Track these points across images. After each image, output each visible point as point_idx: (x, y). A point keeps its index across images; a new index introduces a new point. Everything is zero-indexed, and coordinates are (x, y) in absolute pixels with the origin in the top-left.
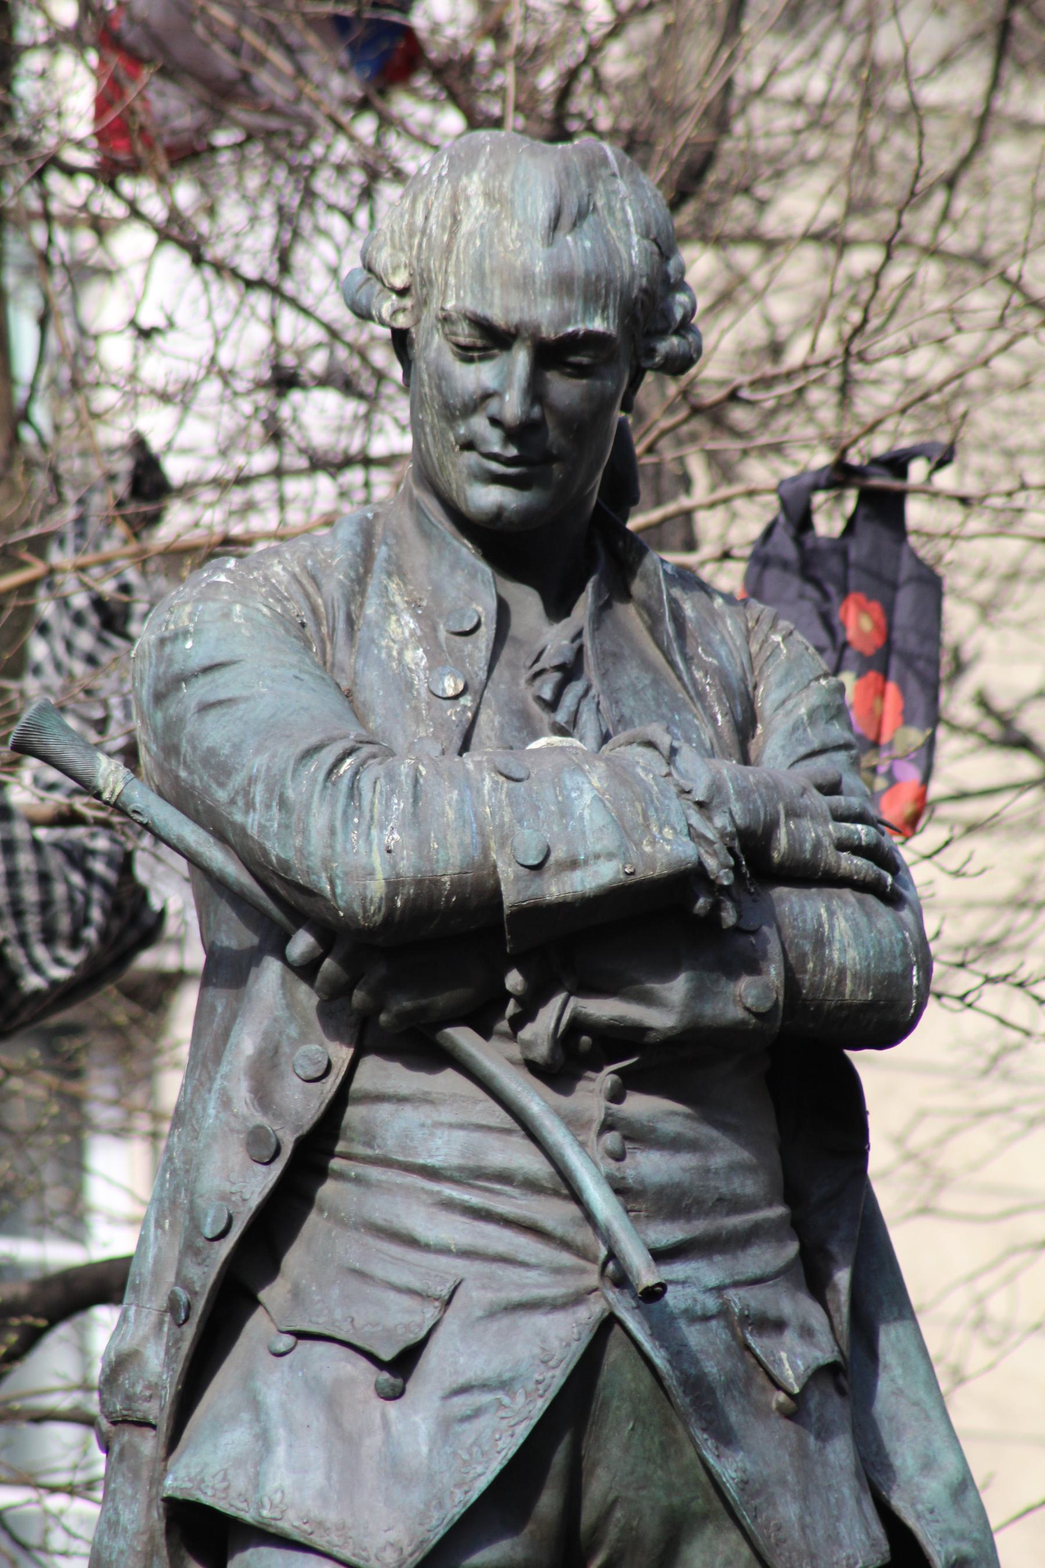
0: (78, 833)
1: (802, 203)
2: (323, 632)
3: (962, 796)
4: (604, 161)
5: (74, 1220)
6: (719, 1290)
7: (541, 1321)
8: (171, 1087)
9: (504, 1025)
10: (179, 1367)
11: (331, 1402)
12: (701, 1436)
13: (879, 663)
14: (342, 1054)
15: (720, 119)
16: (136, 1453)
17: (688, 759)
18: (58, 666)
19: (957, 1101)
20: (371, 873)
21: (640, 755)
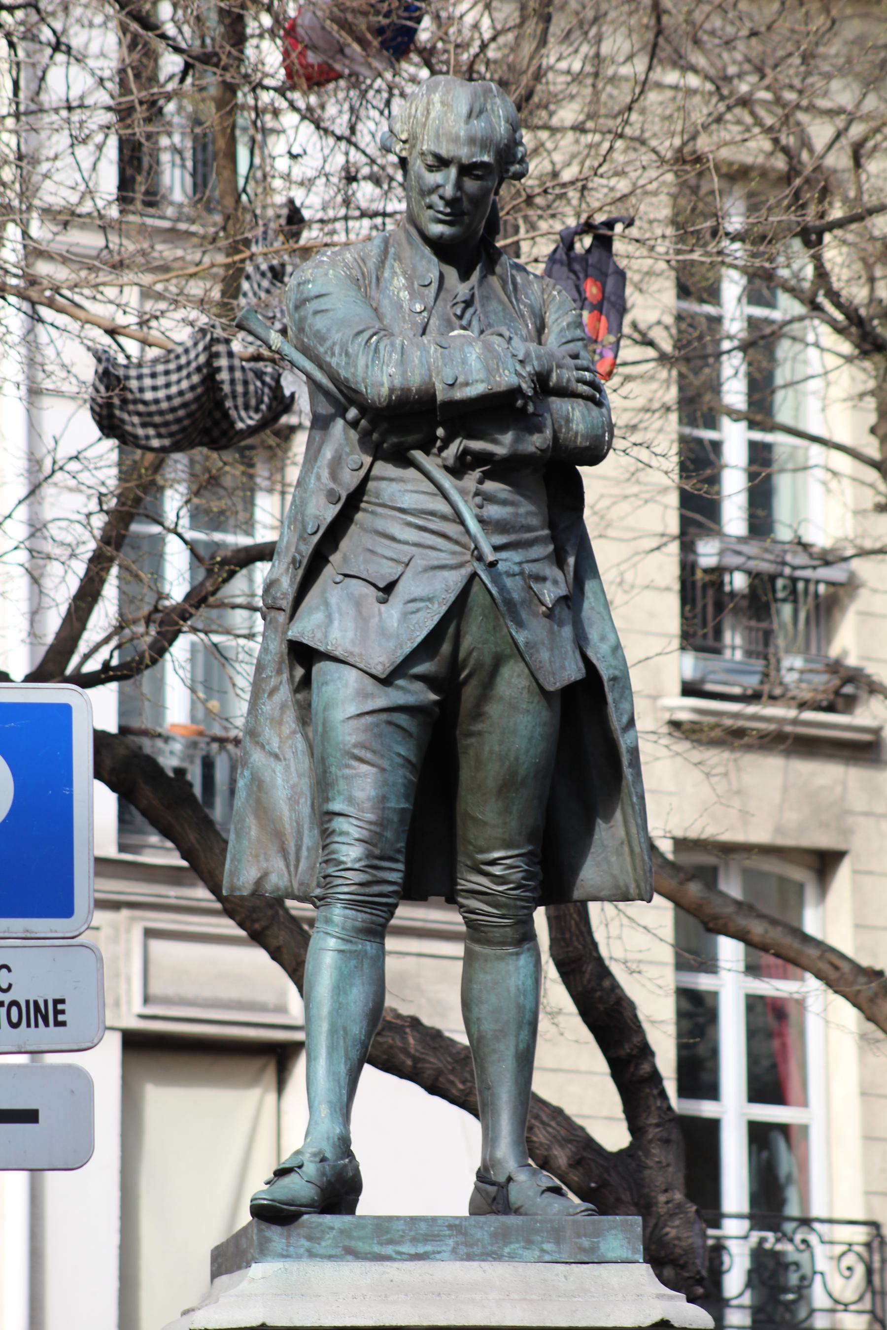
0: (260, 365)
1: (568, 114)
2: (366, 283)
3: (625, 364)
4: (491, 90)
5: (248, 526)
6: (520, 564)
7: (446, 573)
8: (293, 474)
9: (435, 450)
10: (295, 586)
11: (358, 604)
12: (510, 623)
13: (598, 308)
14: (368, 460)
15: (538, 76)
16: (276, 621)
17: (516, 342)
18: (255, 294)
19: (617, 491)
20: (382, 385)
21: (496, 339)
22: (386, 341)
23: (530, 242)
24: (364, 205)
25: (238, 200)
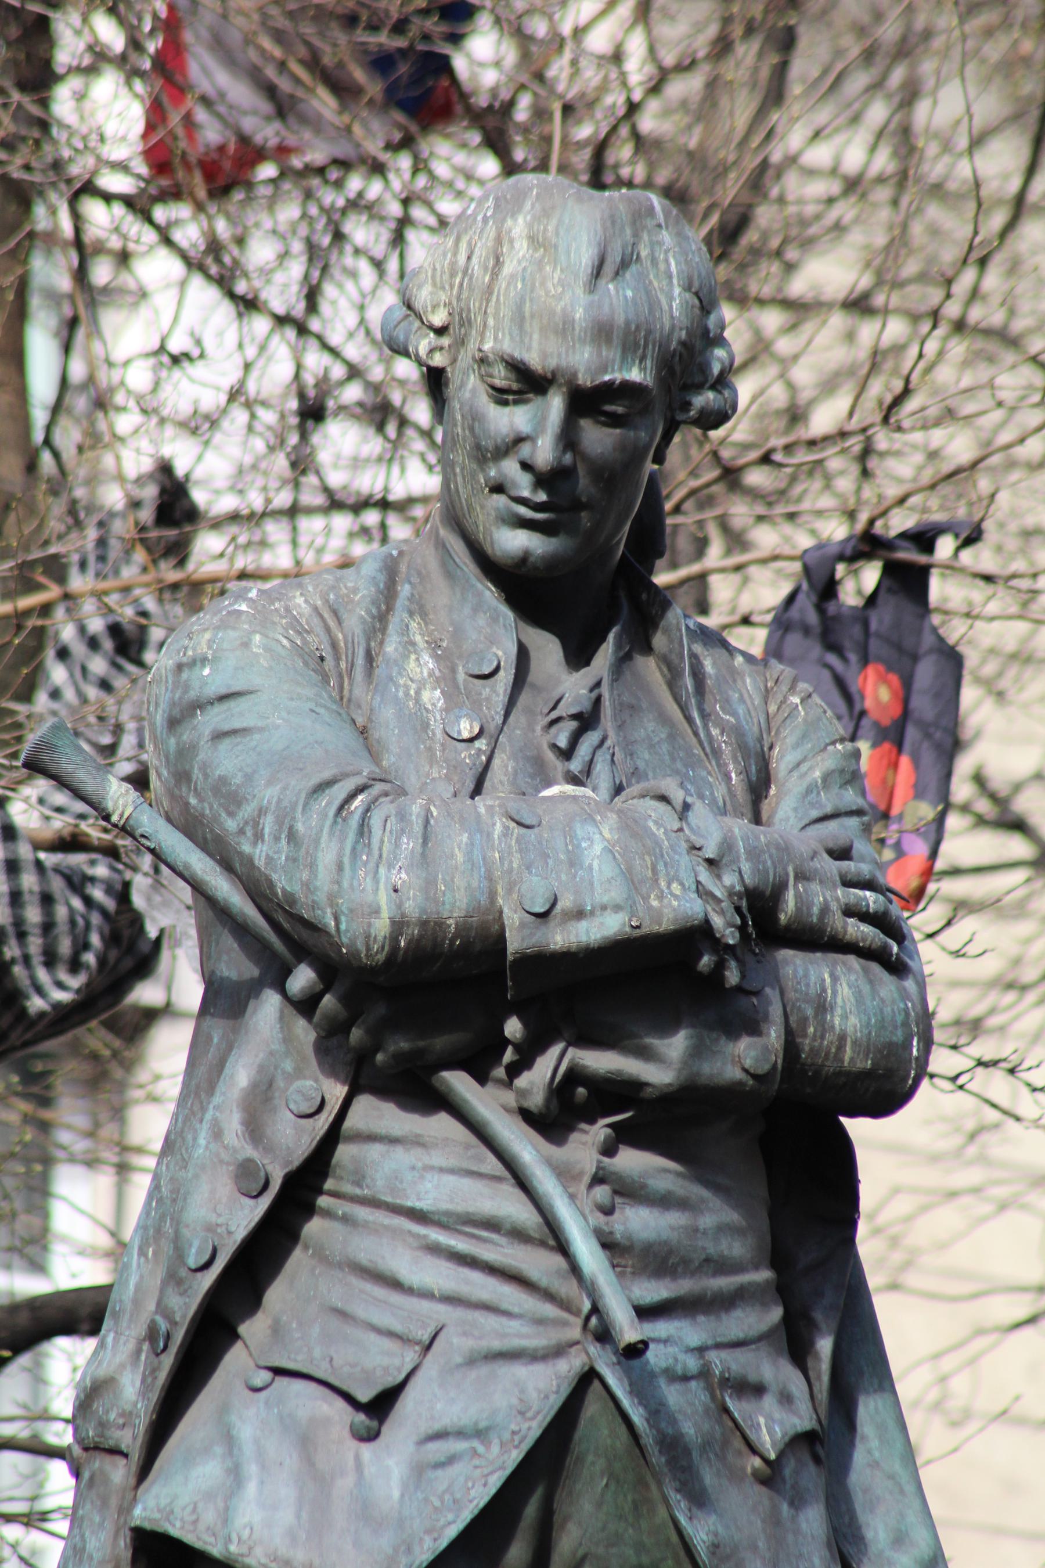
0: (77, 860)
1: (829, 272)
2: (342, 666)
3: (955, 872)
4: (651, 211)
5: (32, 1249)
7: (521, 1371)
8: (150, 1124)
9: (500, 1072)
10: (155, 1396)
11: (306, 1442)
12: (674, 1497)
13: (894, 735)
14: (337, 1091)
15: (759, 181)
16: (106, 1480)
17: (701, 815)
19: (933, 1177)
20: (377, 912)
21: (654, 809)
22: (385, 808)
23: (735, 578)
24: (336, 479)
25: (31, 467)
